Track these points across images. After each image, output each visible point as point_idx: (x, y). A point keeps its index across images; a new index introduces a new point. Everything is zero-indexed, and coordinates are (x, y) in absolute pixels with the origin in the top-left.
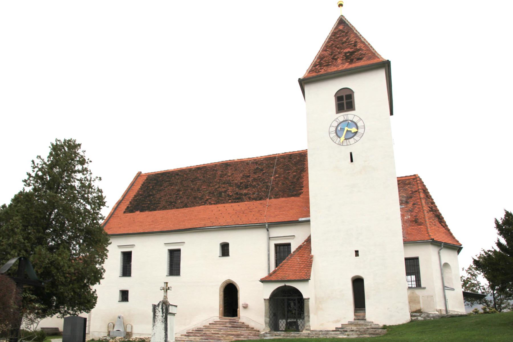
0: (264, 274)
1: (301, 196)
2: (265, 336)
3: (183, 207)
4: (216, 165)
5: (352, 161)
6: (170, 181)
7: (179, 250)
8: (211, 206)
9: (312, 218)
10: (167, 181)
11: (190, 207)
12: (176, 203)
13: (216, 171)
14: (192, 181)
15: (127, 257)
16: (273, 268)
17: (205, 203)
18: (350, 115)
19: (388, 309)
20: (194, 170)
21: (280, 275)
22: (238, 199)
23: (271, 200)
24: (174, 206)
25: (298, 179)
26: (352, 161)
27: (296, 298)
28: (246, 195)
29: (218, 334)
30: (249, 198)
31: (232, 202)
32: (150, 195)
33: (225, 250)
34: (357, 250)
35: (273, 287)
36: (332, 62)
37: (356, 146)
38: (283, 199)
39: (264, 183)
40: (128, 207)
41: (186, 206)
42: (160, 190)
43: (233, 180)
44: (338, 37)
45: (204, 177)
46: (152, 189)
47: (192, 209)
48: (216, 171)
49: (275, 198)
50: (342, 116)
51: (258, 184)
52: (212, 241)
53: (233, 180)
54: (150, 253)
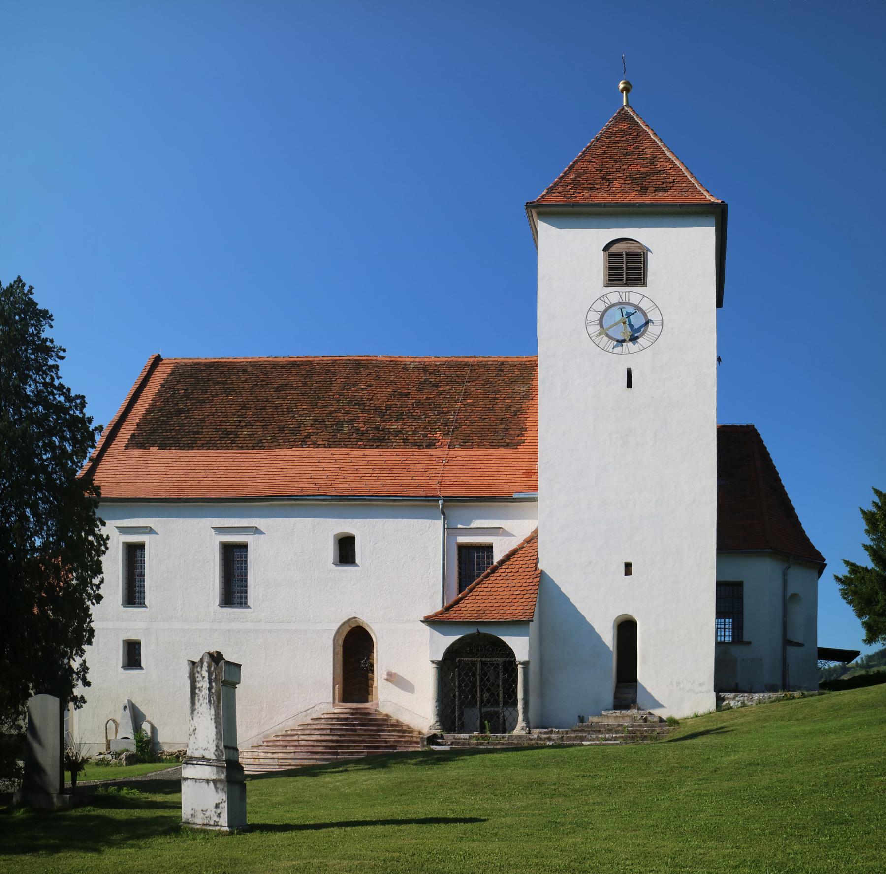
0: (429, 611)
1: (521, 448)
2: (870, 667)
3: (254, 448)
4: (334, 362)
5: (629, 385)
6: (224, 383)
7: (244, 547)
8: (317, 450)
9: (541, 494)
10: (218, 383)
11: (270, 447)
12: (237, 435)
13: (335, 374)
14: (277, 390)
15: (134, 554)
16: (454, 595)
17: (303, 443)
18: (634, 294)
19: (678, 684)
20: (282, 367)
21: (468, 609)
22: (380, 440)
23: (452, 451)
24: (233, 442)
25: (515, 414)
26: (629, 385)
27: (500, 660)
28: (398, 433)
29: (273, 753)
30: (405, 441)
31: (365, 447)
32: (180, 412)
33: (346, 551)
34: (628, 561)
35: (447, 641)
36: (601, 184)
37: (635, 356)
38: (482, 451)
39: (439, 413)
40: (133, 435)
41: (259, 445)
42: (203, 402)
43: (371, 399)
44: (618, 142)
45: (305, 384)
46: (183, 396)
47: (274, 452)
48: (335, 374)
49: (462, 446)
50: (615, 294)
51: (425, 414)
52: (320, 532)
53: (371, 399)
54: (184, 549)
